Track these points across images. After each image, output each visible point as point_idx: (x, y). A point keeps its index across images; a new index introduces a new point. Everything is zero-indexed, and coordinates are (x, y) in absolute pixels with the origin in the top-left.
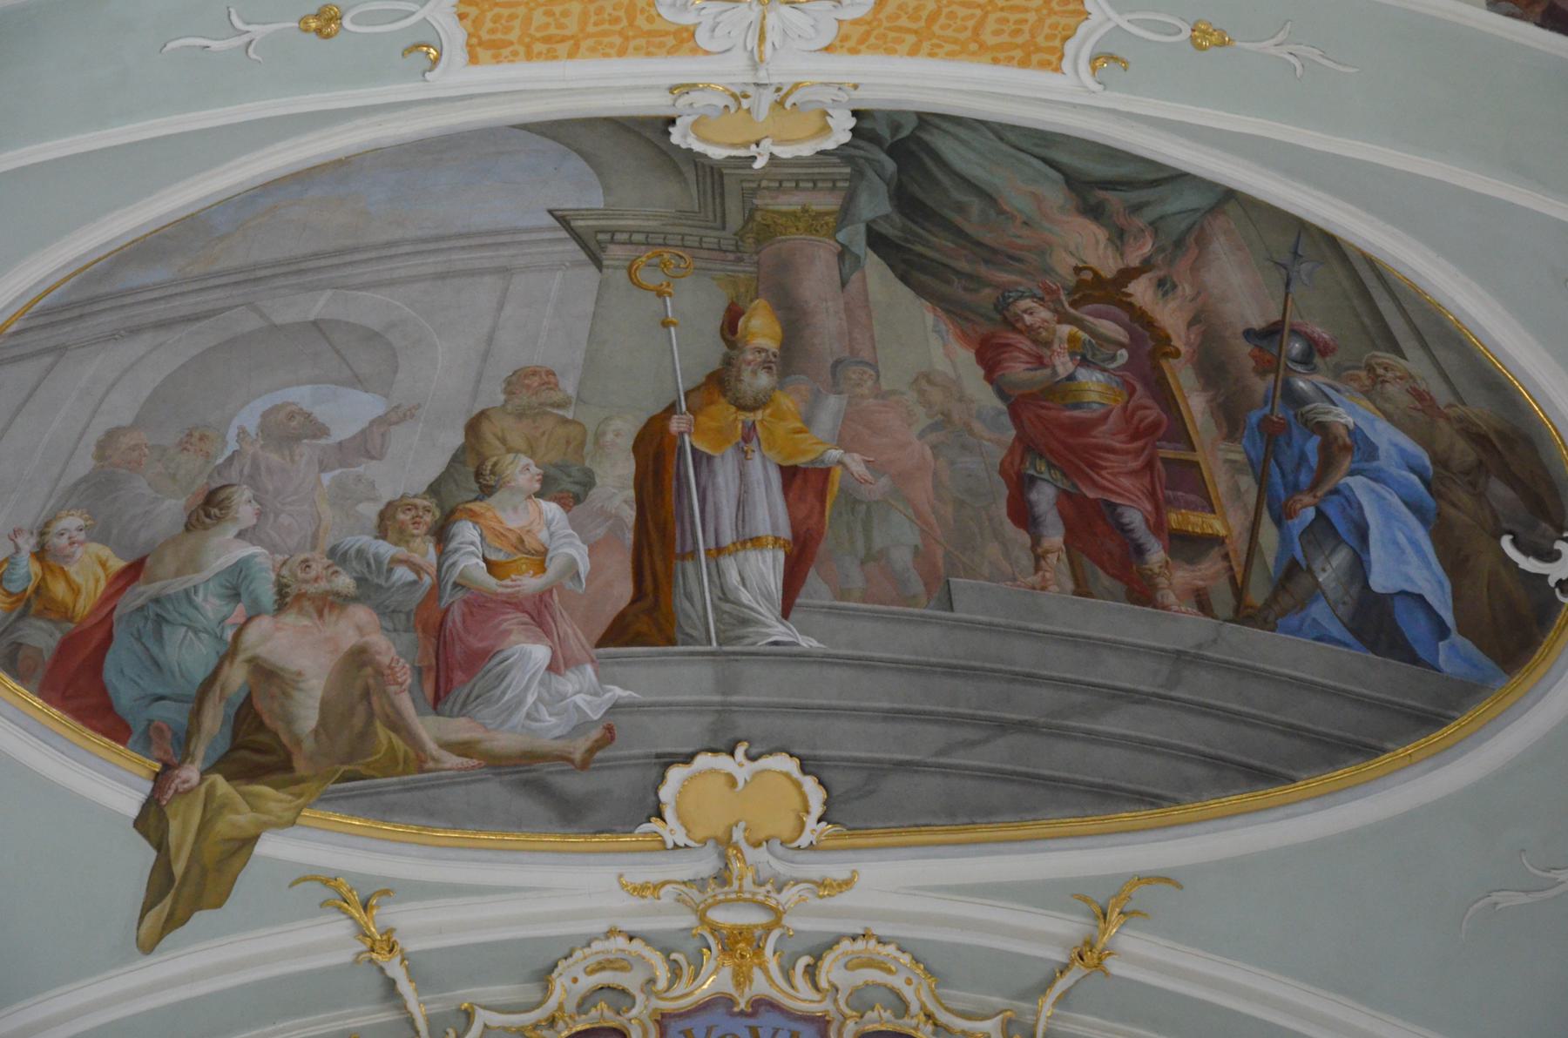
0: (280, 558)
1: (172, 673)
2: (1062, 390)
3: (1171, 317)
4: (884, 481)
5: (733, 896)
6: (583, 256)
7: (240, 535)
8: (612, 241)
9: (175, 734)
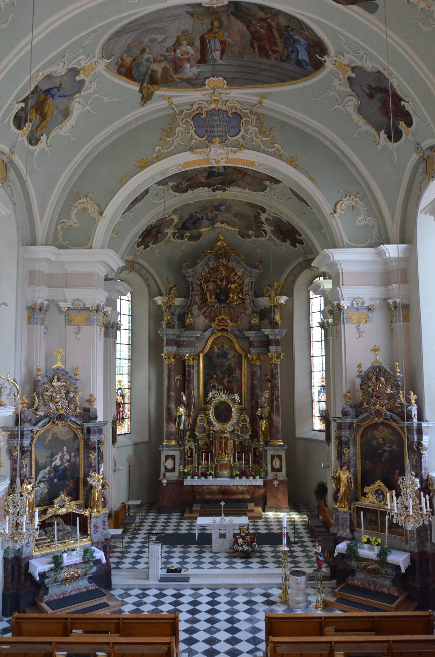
2: (258, 32)
3: (273, 24)
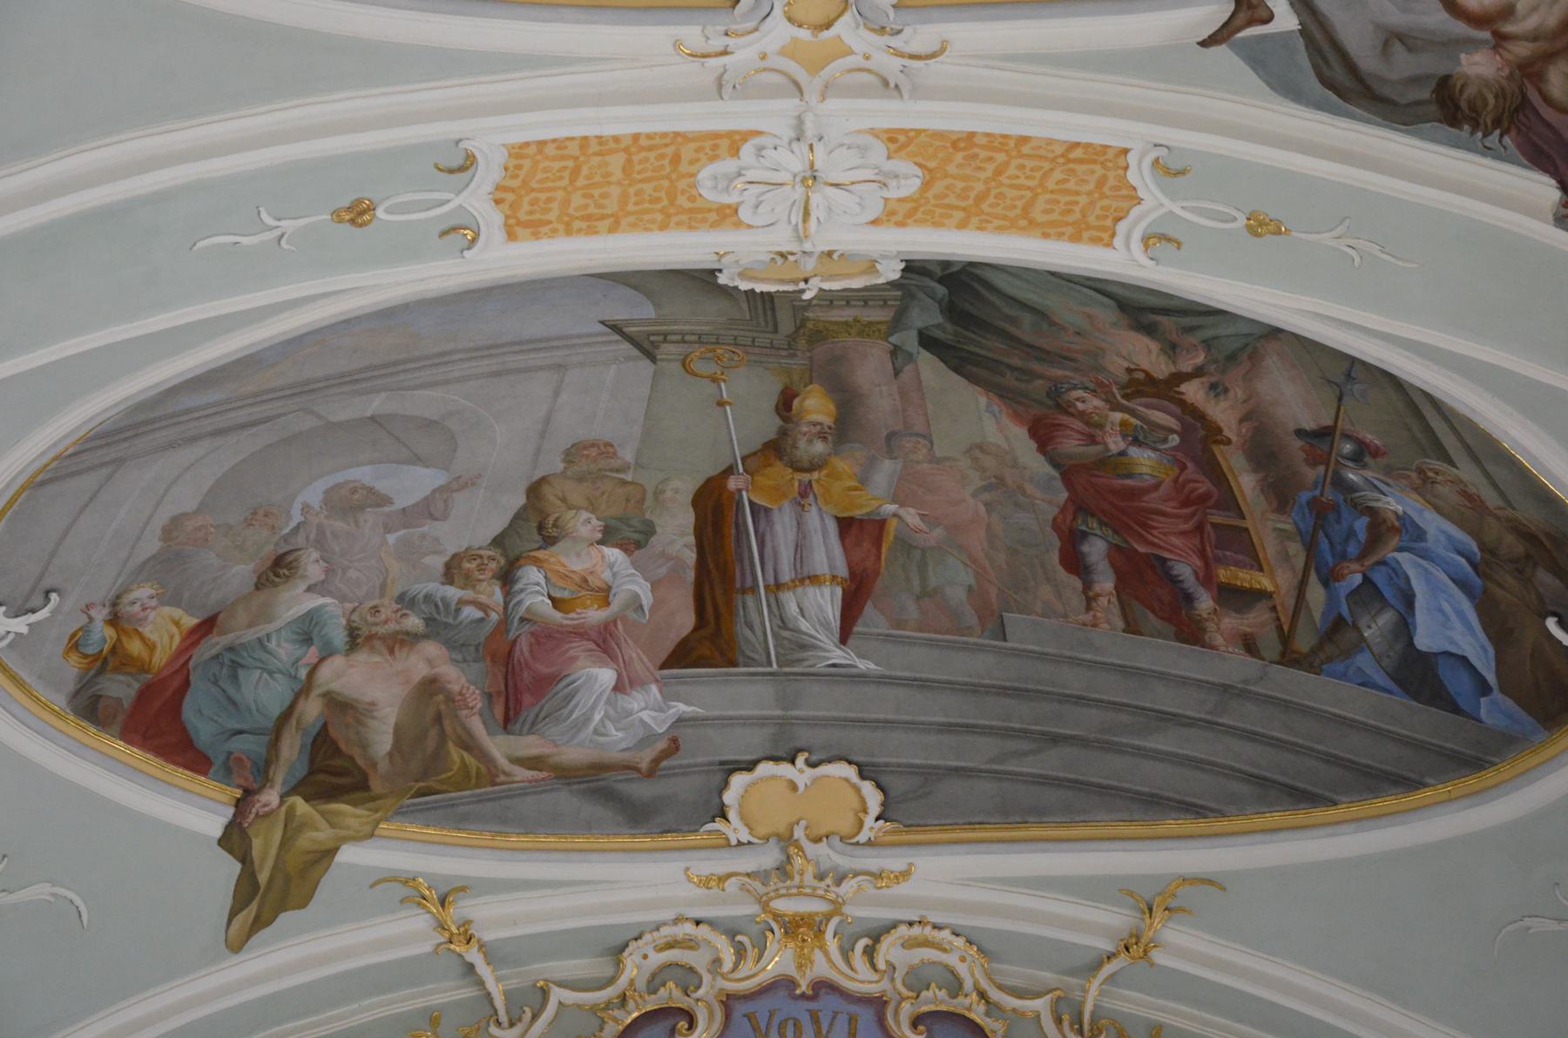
0: (349, 606)
1: (250, 711)
2: (1115, 464)
3: (1223, 413)
4: (938, 532)
5: (794, 891)
6: (636, 353)
7: (309, 589)
8: (665, 341)
9: (255, 763)
